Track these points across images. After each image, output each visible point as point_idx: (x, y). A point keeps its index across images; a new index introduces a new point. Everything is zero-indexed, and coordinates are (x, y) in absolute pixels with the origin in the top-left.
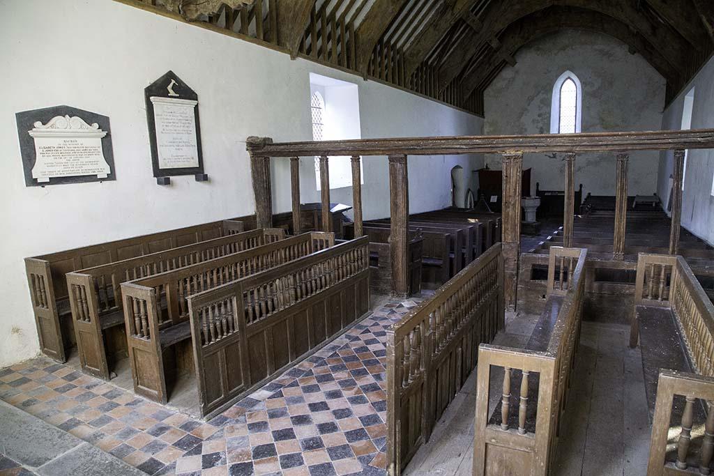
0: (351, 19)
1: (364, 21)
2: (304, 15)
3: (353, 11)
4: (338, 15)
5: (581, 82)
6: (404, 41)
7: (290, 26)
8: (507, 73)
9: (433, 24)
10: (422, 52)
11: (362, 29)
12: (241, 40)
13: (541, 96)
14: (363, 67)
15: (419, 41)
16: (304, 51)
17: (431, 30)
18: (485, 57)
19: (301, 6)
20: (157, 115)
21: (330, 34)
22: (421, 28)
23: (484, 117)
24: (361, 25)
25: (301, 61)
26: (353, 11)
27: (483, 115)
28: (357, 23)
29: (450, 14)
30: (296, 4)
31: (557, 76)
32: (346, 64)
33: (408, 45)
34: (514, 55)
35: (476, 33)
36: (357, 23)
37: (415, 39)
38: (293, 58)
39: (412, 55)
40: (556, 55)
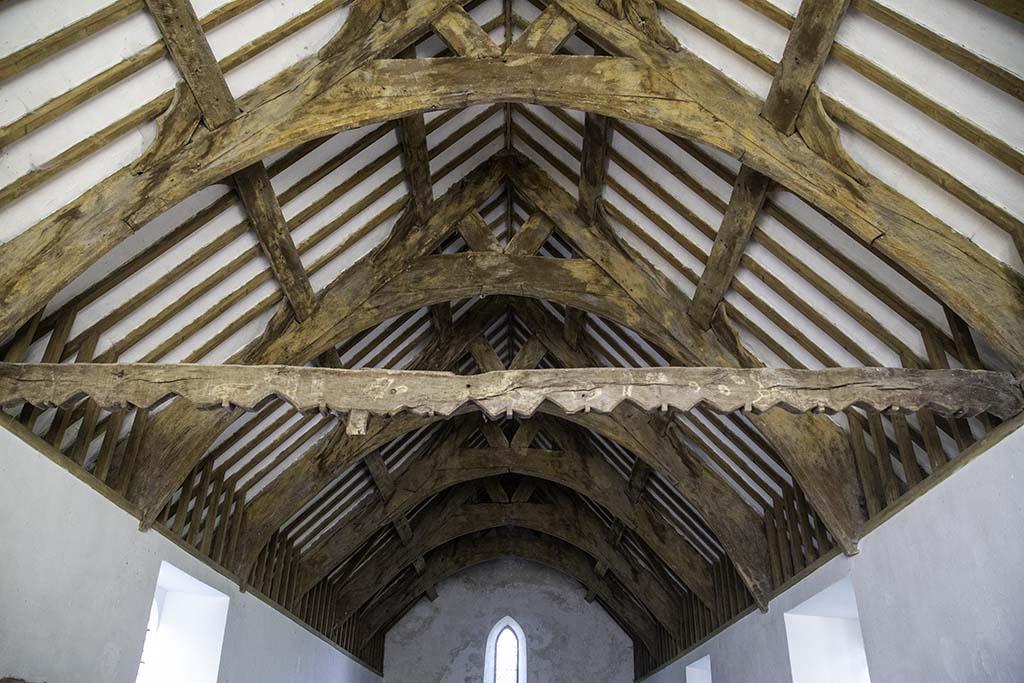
0: (244, 486)
1: (262, 494)
2: (188, 460)
3: (250, 475)
4: (228, 474)
5: (525, 633)
6: (305, 541)
7: (156, 471)
8: (422, 610)
9: (354, 522)
10: (330, 559)
11: (255, 507)
12: (66, 472)
13: (470, 650)
14: (244, 568)
15: (327, 543)
16: (164, 518)
17: (349, 530)
18: (401, 582)
19: (188, 444)
20: (629, 653)
21: (209, 498)
22: (333, 524)
23: (382, 676)
24: (255, 499)
25: (154, 536)
26: (250, 475)
27: (382, 671)
28: (250, 495)
29: (381, 511)
30: (180, 438)
31: (494, 623)
32: (220, 559)
33: (309, 545)
34: (597, 598)
35: (402, 545)
36: (250, 495)
37: (322, 537)
38: (144, 527)
39: (312, 562)
40: (492, 591)
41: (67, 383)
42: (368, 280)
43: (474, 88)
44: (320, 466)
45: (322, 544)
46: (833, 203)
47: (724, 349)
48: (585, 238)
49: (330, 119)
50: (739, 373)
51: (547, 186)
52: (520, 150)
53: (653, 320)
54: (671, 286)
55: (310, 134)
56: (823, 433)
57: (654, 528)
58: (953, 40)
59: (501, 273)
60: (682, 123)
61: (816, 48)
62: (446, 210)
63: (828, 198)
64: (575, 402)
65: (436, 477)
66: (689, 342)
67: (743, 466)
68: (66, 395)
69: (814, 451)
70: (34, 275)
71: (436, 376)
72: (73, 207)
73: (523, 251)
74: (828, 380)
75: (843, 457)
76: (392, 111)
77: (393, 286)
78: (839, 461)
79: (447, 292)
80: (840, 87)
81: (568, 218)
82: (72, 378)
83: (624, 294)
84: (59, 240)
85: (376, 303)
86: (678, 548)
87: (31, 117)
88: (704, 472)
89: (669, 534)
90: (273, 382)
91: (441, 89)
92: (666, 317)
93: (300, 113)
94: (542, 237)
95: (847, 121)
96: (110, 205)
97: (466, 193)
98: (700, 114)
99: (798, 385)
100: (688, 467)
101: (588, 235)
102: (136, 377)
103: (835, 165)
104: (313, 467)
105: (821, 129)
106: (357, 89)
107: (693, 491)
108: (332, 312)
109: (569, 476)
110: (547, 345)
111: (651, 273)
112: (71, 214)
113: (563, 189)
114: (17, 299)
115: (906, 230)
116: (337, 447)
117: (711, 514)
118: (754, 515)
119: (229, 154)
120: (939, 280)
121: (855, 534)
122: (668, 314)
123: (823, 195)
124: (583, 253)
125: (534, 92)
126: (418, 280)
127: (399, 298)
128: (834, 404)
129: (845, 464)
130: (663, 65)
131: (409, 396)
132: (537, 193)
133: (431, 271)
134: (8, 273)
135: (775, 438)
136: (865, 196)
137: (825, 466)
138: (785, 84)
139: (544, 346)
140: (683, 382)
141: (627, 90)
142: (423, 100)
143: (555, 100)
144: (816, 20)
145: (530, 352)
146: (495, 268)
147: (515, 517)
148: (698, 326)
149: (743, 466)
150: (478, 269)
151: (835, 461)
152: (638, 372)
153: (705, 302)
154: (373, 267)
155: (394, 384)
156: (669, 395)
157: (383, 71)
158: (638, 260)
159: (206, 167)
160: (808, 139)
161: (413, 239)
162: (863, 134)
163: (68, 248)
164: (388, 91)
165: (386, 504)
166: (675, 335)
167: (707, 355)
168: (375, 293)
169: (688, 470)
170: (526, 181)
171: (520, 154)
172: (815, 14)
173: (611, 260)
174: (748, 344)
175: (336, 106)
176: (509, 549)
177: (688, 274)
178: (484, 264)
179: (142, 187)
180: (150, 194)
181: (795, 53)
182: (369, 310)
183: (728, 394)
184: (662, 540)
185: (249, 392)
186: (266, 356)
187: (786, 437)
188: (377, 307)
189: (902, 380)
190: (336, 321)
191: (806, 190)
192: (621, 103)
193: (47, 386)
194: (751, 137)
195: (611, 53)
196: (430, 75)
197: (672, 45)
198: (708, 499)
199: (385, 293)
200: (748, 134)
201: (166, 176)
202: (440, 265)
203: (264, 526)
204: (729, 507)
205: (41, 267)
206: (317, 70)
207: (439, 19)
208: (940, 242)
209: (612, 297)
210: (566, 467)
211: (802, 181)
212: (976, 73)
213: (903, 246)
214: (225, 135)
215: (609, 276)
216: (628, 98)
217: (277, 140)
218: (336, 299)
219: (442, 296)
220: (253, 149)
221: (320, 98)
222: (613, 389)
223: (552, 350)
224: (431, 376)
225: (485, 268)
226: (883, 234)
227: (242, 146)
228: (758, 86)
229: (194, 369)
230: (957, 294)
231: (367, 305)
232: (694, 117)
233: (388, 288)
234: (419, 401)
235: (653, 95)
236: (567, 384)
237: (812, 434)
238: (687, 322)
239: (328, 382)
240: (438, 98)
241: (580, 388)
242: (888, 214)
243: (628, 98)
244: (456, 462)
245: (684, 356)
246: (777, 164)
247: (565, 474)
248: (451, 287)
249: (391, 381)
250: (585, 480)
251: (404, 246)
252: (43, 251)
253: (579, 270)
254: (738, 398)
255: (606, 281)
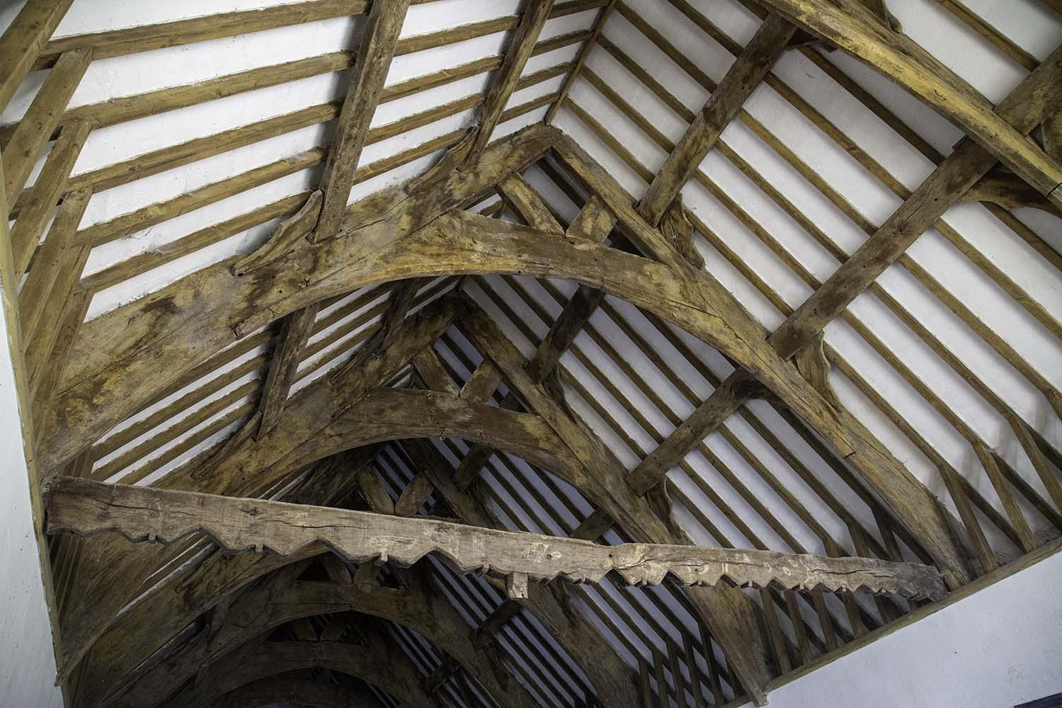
15: (131, 688)
29: (202, 650)
41: (181, 516)
42: (328, 403)
43: (553, 263)
44: (187, 598)
45: (125, 688)
46: (821, 423)
47: (654, 515)
48: (534, 394)
49: (432, 262)
50: (793, 558)
51: (496, 336)
52: (470, 295)
53: (598, 483)
54: (609, 453)
55: (412, 273)
56: (733, 597)
57: (497, 676)
58: (931, 332)
59: (461, 418)
60: (715, 335)
61: (835, 308)
62: (402, 342)
63: (817, 417)
64: (690, 575)
65: (270, 612)
66: (627, 507)
67: (627, 620)
68: (181, 530)
69: (729, 613)
70: (130, 374)
71: (585, 545)
72: (163, 296)
73: (477, 397)
74: (845, 567)
75: (749, 619)
76: (485, 268)
77: (354, 414)
78: (747, 623)
79: (410, 429)
80: (836, 337)
81: (517, 371)
82: (187, 510)
83: (572, 455)
84: (155, 335)
85: (338, 429)
86: (519, 697)
87: (187, 199)
88: (582, 624)
89: (510, 681)
90: (434, 539)
91: (525, 257)
92: (607, 480)
93: (400, 249)
94: (493, 387)
95: (837, 363)
96: (212, 306)
97: (422, 327)
98: (725, 329)
99: (829, 570)
100: (568, 617)
101: (536, 391)
102: (275, 518)
103: (818, 391)
104: (178, 599)
105: (816, 363)
106: (450, 236)
107: (573, 642)
108: (291, 433)
109: (414, 619)
110: (436, 485)
111: (591, 437)
112: (161, 306)
113: (511, 343)
114: (109, 403)
115: (867, 451)
116: (207, 575)
117: (589, 664)
118: (625, 668)
119: (337, 276)
120: (892, 493)
121: (764, 688)
122: (609, 479)
123: (814, 415)
124: (530, 406)
125: (602, 280)
126: (380, 412)
127: (362, 428)
128: (851, 586)
129: (751, 626)
130: (693, 279)
131: (563, 562)
132: (488, 341)
133: (393, 404)
134: (92, 365)
135: (699, 600)
136: (840, 420)
137: (738, 626)
138: (798, 324)
139: (433, 484)
140: (759, 563)
141: (672, 296)
142: (512, 264)
143: (619, 291)
144: (843, 290)
145: (417, 489)
146: (453, 411)
147: (325, 657)
148: (634, 492)
149: (627, 620)
150: (438, 410)
151: (744, 623)
152: (729, 552)
153: (649, 473)
154: (332, 390)
155: (549, 549)
156: (753, 573)
157: (469, 223)
158: (579, 423)
159: (315, 284)
160: (802, 368)
161: (373, 365)
162: (846, 374)
163: (170, 347)
164: (479, 247)
165: (212, 639)
166: (616, 498)
167: (643, 520)
168: (335, 418)
169: (568, 621)
170: (477, 327)
171: (470, 299)
172: (844, 285)
173: (558, 420)
174: (679, 516)
175: (434, 250)
176: (292, 693)
177: (632, 445)
178: (445, 405)
179: (248, 292)
180: (258, 302)
181: (816, 306)
182: (331, 436)
183: (789, 574)
184: (504, 688)
185: (410, 547)
186: (218, 474)
187: (708, 600)
188: (340, 435)
189: (884, 570)
190: (296, 444)
191: (803, 408)
192: (670, 307)
193: (151, 516)
194: (764, 358)
195: (644, 254)
196: (513, 240)
197: (699, 263)
198: (587, 651)
199: (347, 420)
200: (761, 354)
201: (273, 285)
202: (401, 400)
203: (110, 670)
204: (604, 658)
205: (137, 366)
206: (406, 204)
207: (504, 181)
208: (887, 463)
209: (562, 455)
210: (410, 608)
211: (800, 401)
212: (943, 357)
213: (868, 464)
214: (329, 252)
215: (557, 435)
216: (674, 304)
217: (384, 272)
218: (294, 420)
219: (405, 433)
220: (362, 277)
221: (416, 236)
222: (716, 566)
223: (439, 488)
224: (579, 544)
225: (445, 410)
226: (855, 453)
227: (348, 269)
228: (766, 317)
229: (344, 516)
230: (904, 506)
231: (328, 431)
232: (721, 332)
233: (349, 416)
234: (572, 567)
235: (691, 305)
236: (683, 559)
237: (726, 598)
238: (624, 487)
239: (487, 543)
240: (525, 265)
241: (694, 563)
242: (856, 437)
243: (674, 304)
244: (293, 596)
245: (623, 519)
246: (782, 384)
247: (410, 615)
248: (413, 425)
249: (546, 546)
250: (429, 623)
251: (362, 372)
252: (137, 345)
253: (531, 424)
254: (795, 578)
255: (555, 440)
